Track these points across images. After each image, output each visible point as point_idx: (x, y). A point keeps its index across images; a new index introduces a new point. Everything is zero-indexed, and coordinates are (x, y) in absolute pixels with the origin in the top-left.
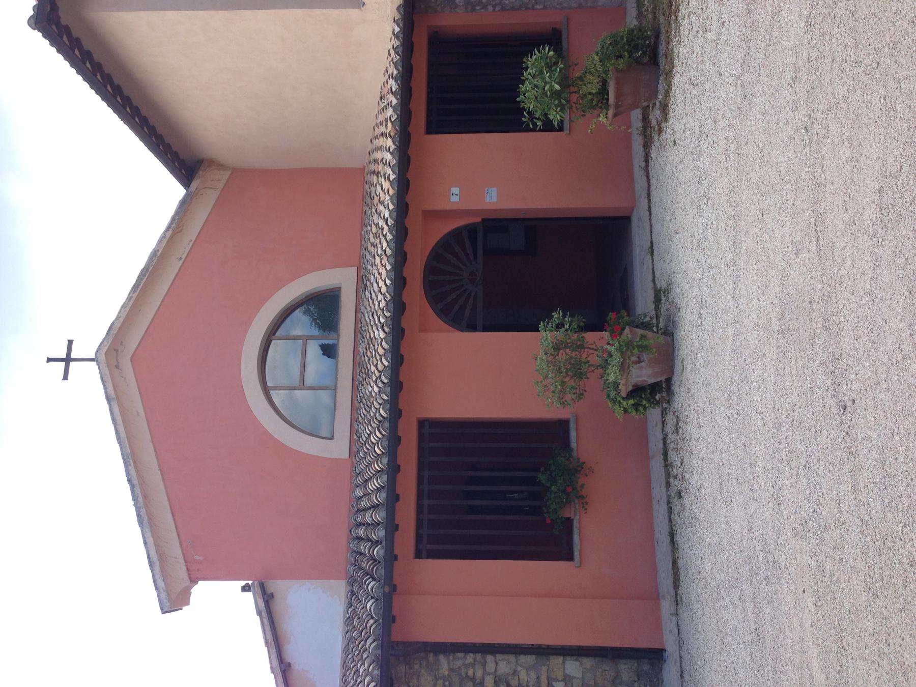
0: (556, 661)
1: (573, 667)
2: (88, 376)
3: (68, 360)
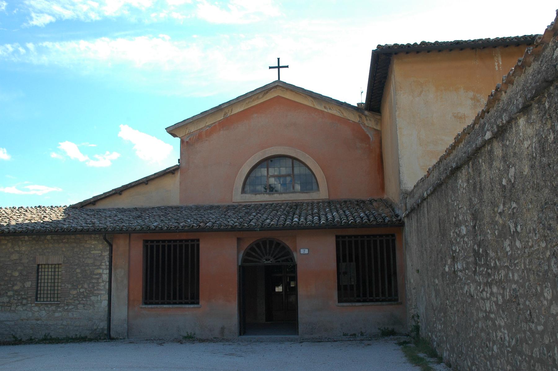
1: (105, 303)
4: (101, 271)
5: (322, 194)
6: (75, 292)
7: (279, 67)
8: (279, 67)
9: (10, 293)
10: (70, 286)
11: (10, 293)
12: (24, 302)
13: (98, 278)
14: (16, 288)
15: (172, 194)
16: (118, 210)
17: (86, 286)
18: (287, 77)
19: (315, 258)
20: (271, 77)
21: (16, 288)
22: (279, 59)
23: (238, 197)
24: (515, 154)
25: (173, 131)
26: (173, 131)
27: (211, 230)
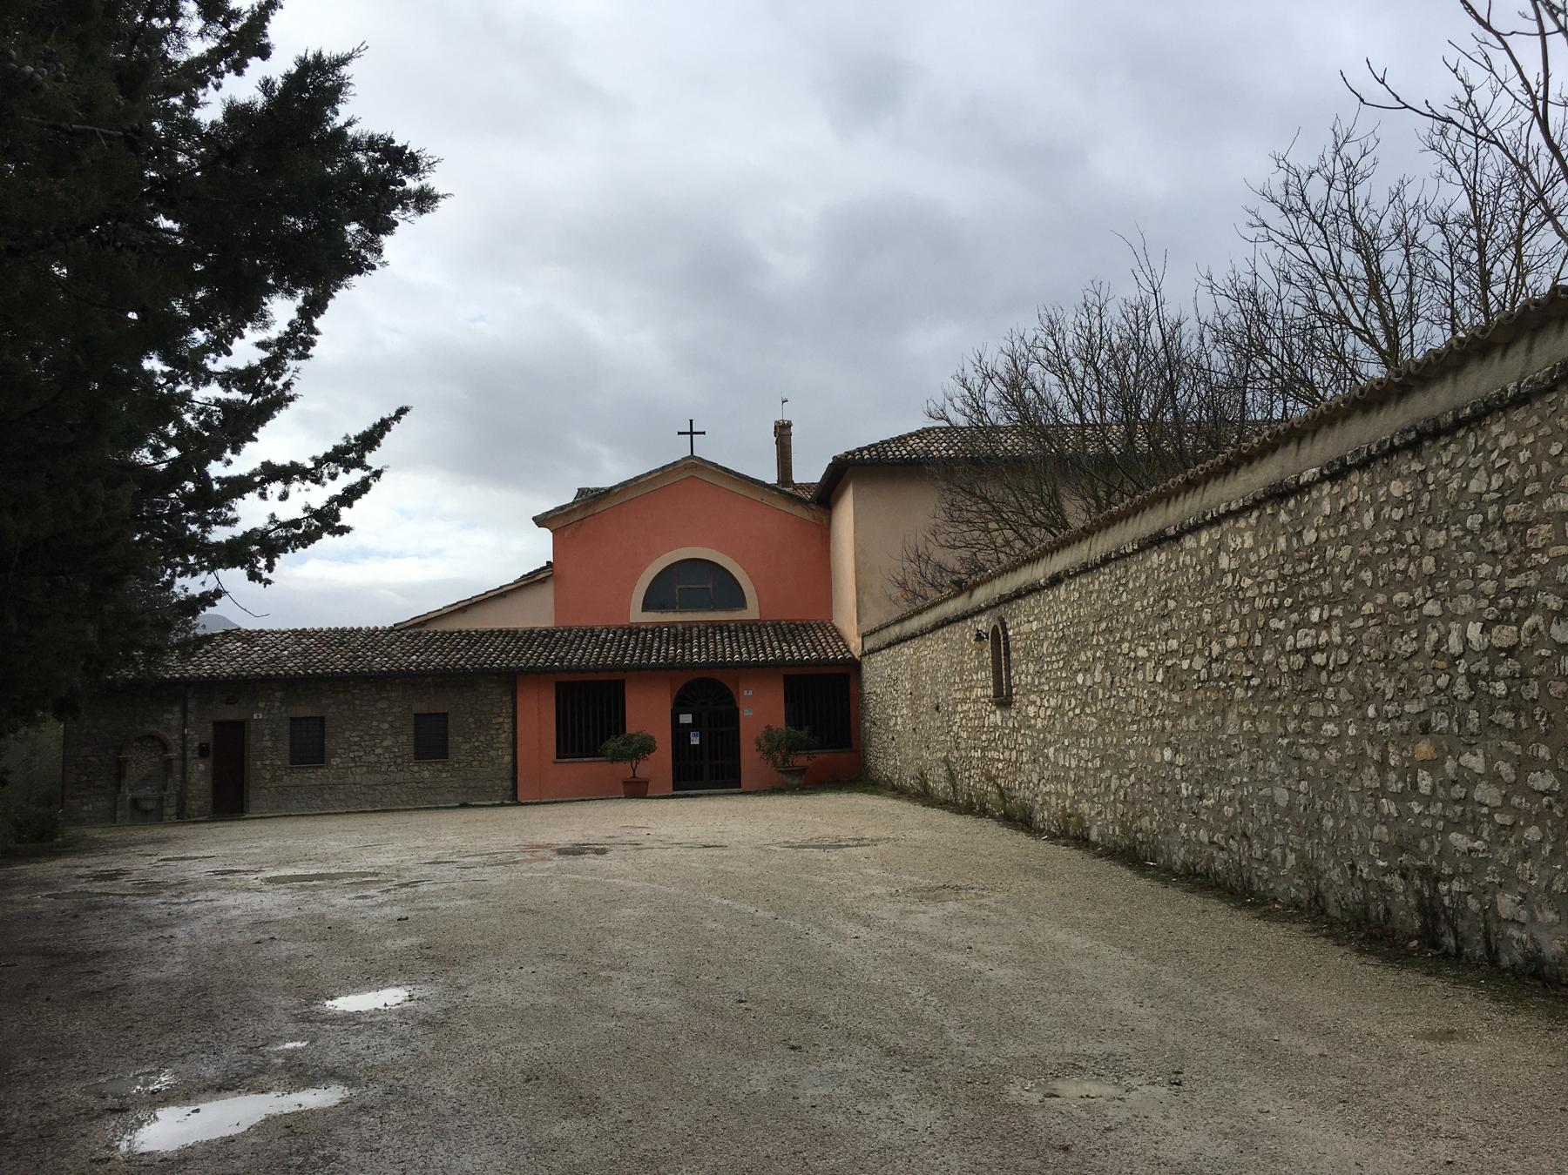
0: (510, 751)
1: (508, 758)
2: (679, 450)
3: (692, 433)
5: (752, 612)
7: (692, 433)
11: (378, 751)
14: (385, 743)
15: (537, 613)
19: (760, 712)
21: (385, 743)
23: (638, 616)
25: (541, 521)
26: (541, 521)
27: (640, 670)
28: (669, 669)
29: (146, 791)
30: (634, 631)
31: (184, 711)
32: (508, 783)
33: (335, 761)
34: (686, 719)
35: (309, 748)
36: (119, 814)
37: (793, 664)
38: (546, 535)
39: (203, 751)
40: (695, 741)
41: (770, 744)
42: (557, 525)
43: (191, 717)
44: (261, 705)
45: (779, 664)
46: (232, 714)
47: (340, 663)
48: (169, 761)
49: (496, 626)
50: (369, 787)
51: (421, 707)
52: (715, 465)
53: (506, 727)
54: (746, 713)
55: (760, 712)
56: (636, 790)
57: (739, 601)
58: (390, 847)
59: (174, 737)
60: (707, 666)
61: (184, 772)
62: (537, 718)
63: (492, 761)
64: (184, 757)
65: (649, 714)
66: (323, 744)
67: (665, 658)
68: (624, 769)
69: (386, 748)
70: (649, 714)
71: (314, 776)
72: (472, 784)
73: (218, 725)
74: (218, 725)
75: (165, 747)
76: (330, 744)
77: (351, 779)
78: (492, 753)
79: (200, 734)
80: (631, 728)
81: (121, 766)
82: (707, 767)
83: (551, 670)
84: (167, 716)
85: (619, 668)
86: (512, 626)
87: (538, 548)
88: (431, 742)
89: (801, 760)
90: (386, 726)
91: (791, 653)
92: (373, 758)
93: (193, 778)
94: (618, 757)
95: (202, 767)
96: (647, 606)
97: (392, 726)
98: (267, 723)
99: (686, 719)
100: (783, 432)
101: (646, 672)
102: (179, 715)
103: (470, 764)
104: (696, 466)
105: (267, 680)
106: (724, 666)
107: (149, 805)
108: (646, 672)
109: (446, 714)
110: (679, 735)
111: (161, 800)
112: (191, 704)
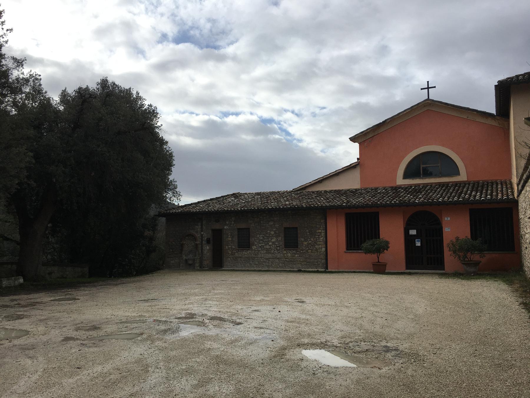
1: (324, 249)
4: (320, 231)
5: (463, 177)
6: (306, 243)
7: (428, 88)
8: (428, 88)
9: (270, 244)
10: (303, 239)
11: (270, 244)
12: (278, 248)
13: (319, 235)
14: (273, 240)
15: (352, 182)
16: (338, 192)
17: (312, 240)
18: (434, 95)
19: (455, 229)
20: (423, 96)
21: (273, 240)
22: (435, 87)
23: (400, 181)
24: (286, 330)
25: (353, 139)
26: (353, 139)
27: (385, 206)
28: (403, 206)
29: (191, 256)
30: (396, 189)
31: (202, 225)
32: (324, 261)
33: (254, 247)
34: (413, 232)
35: (245, 243)
36: (181, 265)
37: (475, 202)
38: (357, 145)
39: (208, 241)
40: (418, 244)
41: (462, 249)
42: (360, 141)
43: (204, 227)
44: (227, 223)
45: (466, 203)
46: (217, 226)
47: (258, 204)
48: (197, 245)
49: (334, 189)
50: (267, 259)
51: (286, 225)
52: (441, 102)
53: (323, 234)
54: (446, 230)
55: (455, 229)
56: (380, 269)
57: (457, 172)
58: (50, 308)
59: (198, 236)
60: (422, 204)
61: (202, 249)
62: (336, 232)
63: (317, 250)
64: (202, 244)
65: (392, 231)
66: (249, 239)
67: (464, 198)
68: (373, 257)
69: (273, 243)
70: (392, 231)
71: (246, 253)
72: (309, 260)
73: (213, 231)
74: (213, 231)
75: (195, 239)
76: (252, 240)
77: (260, 256)
78: (316, 246)
79: (207, 234)
80: (381, 237)
81: (182, 245)
82: (424, 258)
83: (341, 207)
84: (196, 227)
85: (375, 205)
86: (341, 188)
87: (351, 153)
88: (291, 241)
89: (476, 257)
90: (273, 233)
91: (508, 196)
92: (268, 247)
93: (205, 252)
94: (368, 251)
95: (208, 248)
96: (406, 175)
97: (275, 233)
98: (229, 230)
99: (413, 232)
100: (428, 82)
101: (391, 208)
102: (200, 227)
103: (307, 251)
104: (430, 104)
105: (227, 212)
106: (431, 204)
107: (190, 262)
108: (391, 208)
109: (297, 228)
110: (409, 240)
111: (194, 260)
112: (204, 222)
